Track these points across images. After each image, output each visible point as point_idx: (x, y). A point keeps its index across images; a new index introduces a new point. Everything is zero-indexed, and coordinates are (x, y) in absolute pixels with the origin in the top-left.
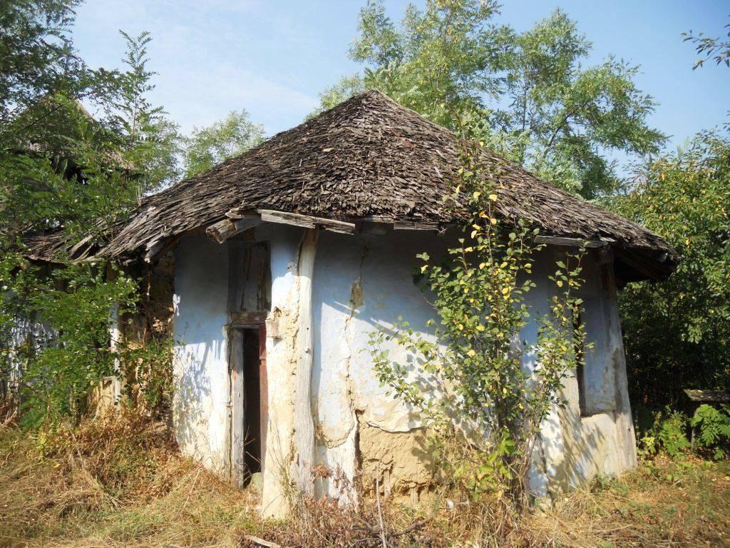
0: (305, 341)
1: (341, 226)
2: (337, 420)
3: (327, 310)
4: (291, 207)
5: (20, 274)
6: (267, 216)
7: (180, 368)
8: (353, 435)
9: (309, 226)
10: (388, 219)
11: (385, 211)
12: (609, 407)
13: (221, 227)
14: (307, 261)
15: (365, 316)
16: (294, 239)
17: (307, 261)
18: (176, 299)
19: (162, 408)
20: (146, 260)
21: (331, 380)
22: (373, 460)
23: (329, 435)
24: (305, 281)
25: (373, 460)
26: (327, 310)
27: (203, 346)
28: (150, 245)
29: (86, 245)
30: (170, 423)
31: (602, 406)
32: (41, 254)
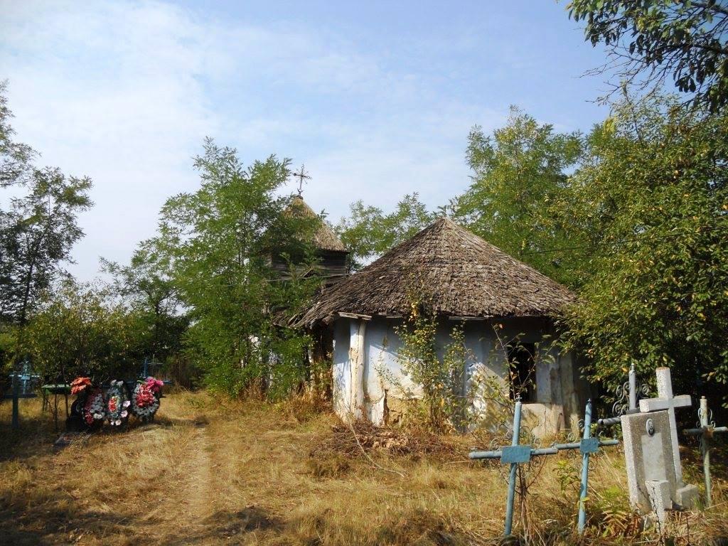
0: (361, 361)
1: (367, 317)
2: (375, 391)
3: (372, 348)
4: (349, 311)
5: (270, 331)
6: (342, 314)
7: (335, 375)
8: (383, 399)
9: (356, 318)
10: (385, 314)
11: (383, 311)
12: (547, 401)
13: (327, 319)
14: (362, 329)
15: (389, 351)
16: (359, 322)
17: (362, 329)
18: (334, 342)
19: (329, 393)
20: (256, 339)
21: (373, 375)
22: (393, 411)
23: (372, 399)
24: (361, 337)
25: (393, 411)
26: (372, 348)
27: (343, 364)
28: (312, 322)
29: (294, 320)
30: (332, 402)
31: (544, 400)
32: (277, 323)
